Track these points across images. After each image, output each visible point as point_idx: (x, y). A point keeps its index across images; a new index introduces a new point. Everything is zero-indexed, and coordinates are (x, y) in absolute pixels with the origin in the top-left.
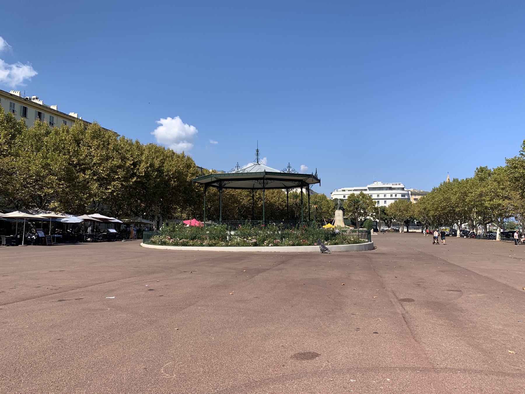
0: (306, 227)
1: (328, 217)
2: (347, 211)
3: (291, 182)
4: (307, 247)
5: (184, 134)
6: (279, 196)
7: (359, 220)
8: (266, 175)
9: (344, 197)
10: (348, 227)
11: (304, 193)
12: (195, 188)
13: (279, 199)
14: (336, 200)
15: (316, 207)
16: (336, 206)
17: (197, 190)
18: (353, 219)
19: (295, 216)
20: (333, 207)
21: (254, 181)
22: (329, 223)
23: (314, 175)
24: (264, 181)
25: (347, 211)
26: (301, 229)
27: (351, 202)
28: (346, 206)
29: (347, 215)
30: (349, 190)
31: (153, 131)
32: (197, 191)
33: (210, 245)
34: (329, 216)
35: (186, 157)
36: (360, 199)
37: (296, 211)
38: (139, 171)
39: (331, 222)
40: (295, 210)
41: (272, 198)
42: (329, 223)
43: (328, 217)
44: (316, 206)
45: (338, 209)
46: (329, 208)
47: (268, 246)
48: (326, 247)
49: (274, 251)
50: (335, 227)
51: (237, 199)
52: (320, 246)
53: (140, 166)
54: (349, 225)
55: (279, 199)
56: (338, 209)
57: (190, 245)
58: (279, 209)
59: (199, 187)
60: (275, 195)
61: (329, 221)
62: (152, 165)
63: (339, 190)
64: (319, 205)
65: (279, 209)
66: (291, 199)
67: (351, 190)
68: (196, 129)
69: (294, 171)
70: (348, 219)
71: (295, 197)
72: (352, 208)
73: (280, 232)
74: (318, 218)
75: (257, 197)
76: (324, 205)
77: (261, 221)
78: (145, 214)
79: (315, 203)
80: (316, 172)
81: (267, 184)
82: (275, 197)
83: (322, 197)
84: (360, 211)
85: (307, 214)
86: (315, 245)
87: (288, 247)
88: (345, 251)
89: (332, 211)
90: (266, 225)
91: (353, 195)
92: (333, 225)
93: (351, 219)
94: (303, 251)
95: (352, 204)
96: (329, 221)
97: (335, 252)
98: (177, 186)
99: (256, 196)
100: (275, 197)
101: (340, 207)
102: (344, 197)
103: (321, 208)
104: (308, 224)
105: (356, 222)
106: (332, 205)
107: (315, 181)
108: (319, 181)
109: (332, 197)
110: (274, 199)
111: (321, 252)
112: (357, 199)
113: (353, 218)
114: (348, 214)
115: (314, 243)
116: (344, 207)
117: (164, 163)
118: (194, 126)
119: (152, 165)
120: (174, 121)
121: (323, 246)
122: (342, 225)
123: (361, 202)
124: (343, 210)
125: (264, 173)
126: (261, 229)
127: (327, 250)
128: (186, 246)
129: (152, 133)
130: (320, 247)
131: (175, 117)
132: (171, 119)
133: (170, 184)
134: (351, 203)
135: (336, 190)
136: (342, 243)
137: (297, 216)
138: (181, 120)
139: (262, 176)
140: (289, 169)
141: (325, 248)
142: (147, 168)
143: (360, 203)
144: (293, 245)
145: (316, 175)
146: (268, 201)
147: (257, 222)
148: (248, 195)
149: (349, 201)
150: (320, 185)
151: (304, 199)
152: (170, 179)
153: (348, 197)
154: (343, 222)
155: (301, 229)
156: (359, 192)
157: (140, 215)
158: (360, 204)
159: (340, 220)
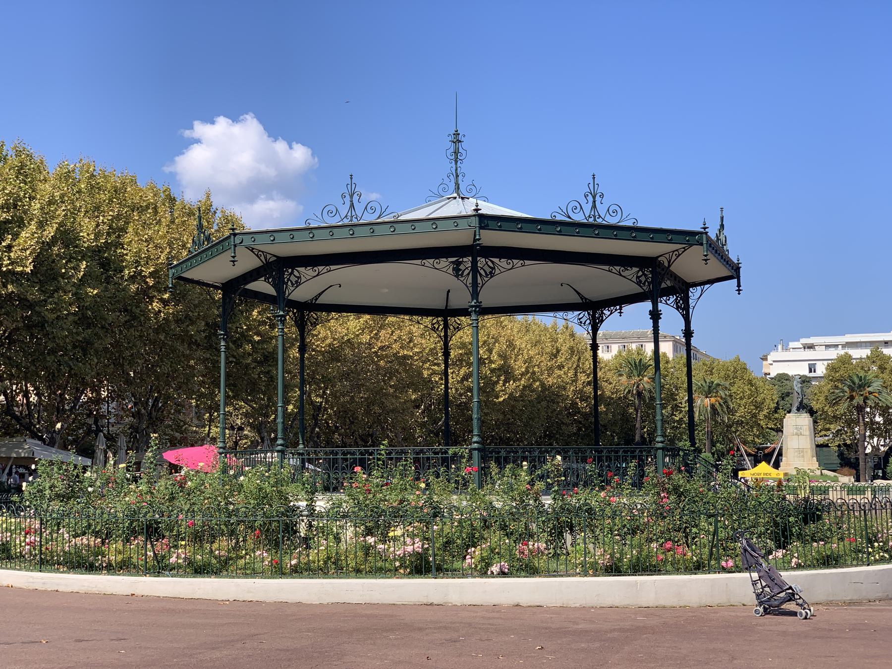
0: (679, 479)
1: (756, 440)
2: (825, 419)
3: (607, 268)
4: (690, 581)
5: (271, 173)
6: (578, 366)
7: (869, 450)
8: (481, 228)
9: (812, 369)
10: (832, 474)
11: (665, 354)
12: (249, 329)
13: (576, 375)
14: (783, 378)
15: (713, 406)
16: (783, 399)
17: (258, 336)
18: (845, 445)
19: (637, 438)
20: (773, 406)
21: (431, 261)
22: (764, 462)
23: (713, 236)
24: (474, 263)
25: (825, 419)
26: (655, 486)
27: (840, 386)
28: (822, 398)
29: (823, 433)
30: (828, 346)
31: (172, 161)
32: (257, 338)
33: (200, 570)
34: (758, 437)
35: (219, 214)
36: (870, 375)
37: (639, 419)
38: (12, 254)
39: (775, 458)
40: (637, 415)
41: (550, 370)
42: (764, 462)
43: (756, 440)
44: (713, 399)
45: (794, 409)
46: (757, 408)
47: (484, 574)
48: (784, 583)
49: (515, 602)
50: (786, 474)
51: (420, 374)
52: (755, 575)
53: (16, 236)
54: (834, 467)
55: (576, 375)
56: (794, 409)
57: (110, 568)
58: (578, 411)
59: (264, 323)
60: (560, 359)
61: (761, 454)
62: (67, 237)
63: (792, 345)
64: (721, 398)
65: (579, 413)
66: (621, 375)
67: (836, 346)
68: (313, 155)
69: (615, 211)
70: (827, 446)
71: (636, 369)
72: (842, 408)
73: (547, 501)
74: (718, 445)
75: (493, 366)
76: (741, 399)
77: (464, 450)
78: (59, 426)
79: (706, 389)
80: (722, 226)
81: (492, 274)
82: (561, 367)
83: (733, 369)
84: (871, 420)
85: (677, 427)
86: (724, 570)
87: (586, 579)
88: (880, 595)
89: (770, 419)
90: (484, 472)
91: (845, 360)
92: (777, 466)
93: (839, 446)
94: (662, 602)
95: (843, 391)
96: (761, 454)
97: (829, 603)
98: (178, 321)
99: (491, 362)
100: (561, 367)
101: (801, 402)
102: (812, 369)
103: (728, 407)
104: (687, 465)
105: (857, 459)
106: (770, 398)
107: (716, 268)
108: (734, 272)
109: (765, 370)
110: (559, 376)
111: (761, 609)
112: (862, 374)
113: (848, 442)
114: (829, 429)
115: (718, 559)
116: (815, 406)
117: (124, 230)
118: (303, 145)
119: (67, 237)
120: (237, 129)
121: (771, 578)
122: (810, 464)
123: (876, 386)
124: (812, 412)
125: (475, 222)
126: (462, 485)
127: (790, 600)
128: (91, 568)
129: (167, 169)
130: (754, 583)
131: (242, 117)
132: (230, 121)
133: (145, 313)
134: (836, 387)
135: (780, 347)
136: (858, 556)
137: (642, 437)
138: (261, 128)
139: (463, 238)
140: (594, 206)
141: (781, 586)
142: (46, 246)
143: (870, 389)
144: (614, 569)
145: (722, 237)
146: (538, 383)
147: (446, 452)
148: (459, 360)
149: (831, 380)
150: (739, 290)
151: (667, 375)
152: (145, 294)
153: (827, 369)
154: (815, 459)
155: (655, 486)
156: (865, 353)
157: (38, 430)
158: (870, 393)
159: (801, 451)
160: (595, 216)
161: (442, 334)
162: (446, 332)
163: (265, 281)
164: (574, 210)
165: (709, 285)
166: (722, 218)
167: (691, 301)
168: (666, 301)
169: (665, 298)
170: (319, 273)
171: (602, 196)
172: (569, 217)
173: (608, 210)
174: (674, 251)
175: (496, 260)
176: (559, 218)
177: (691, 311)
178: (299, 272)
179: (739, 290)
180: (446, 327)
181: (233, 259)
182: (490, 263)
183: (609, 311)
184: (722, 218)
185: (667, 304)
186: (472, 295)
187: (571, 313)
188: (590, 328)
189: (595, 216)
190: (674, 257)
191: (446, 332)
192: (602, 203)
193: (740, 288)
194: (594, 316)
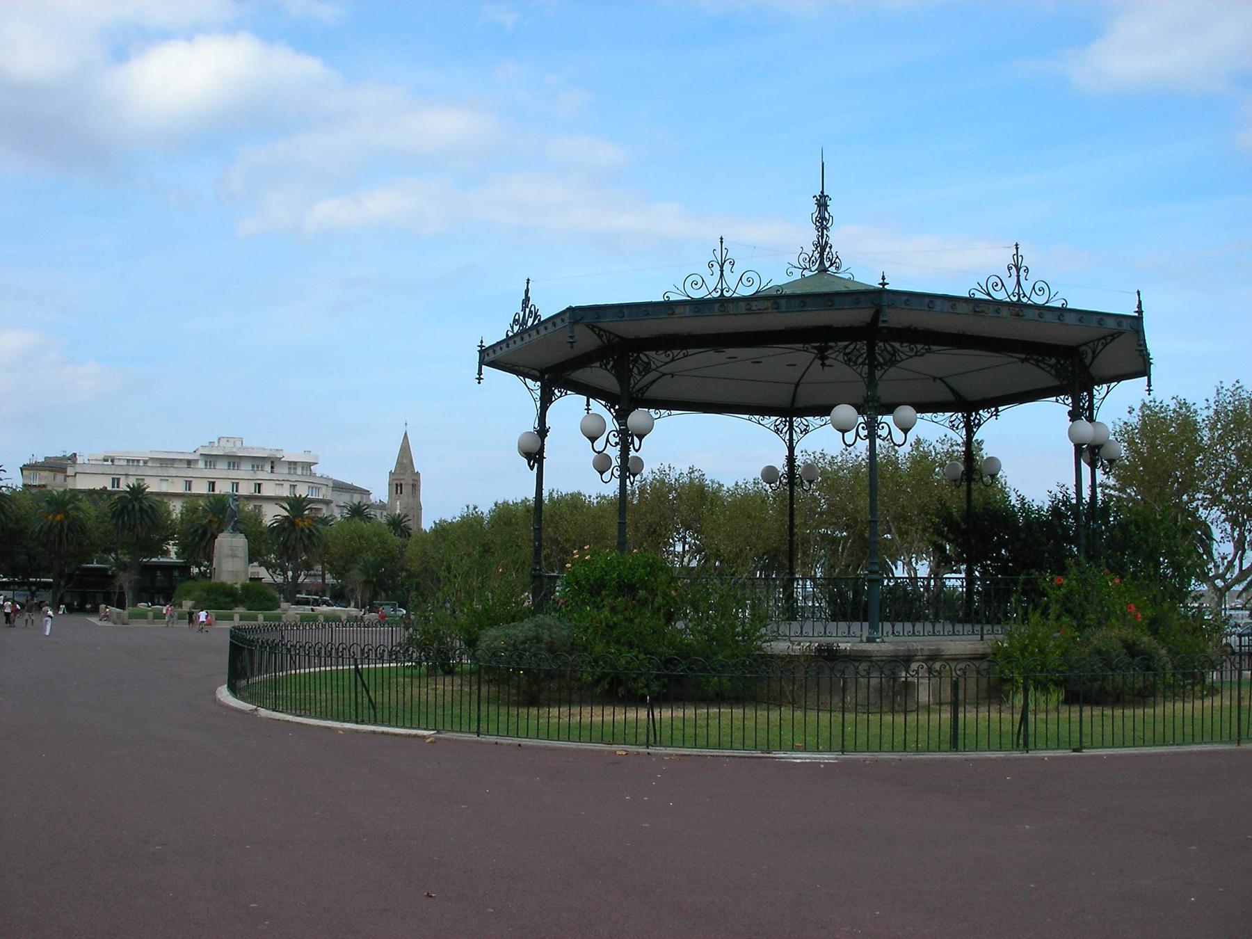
150: (480, 379)
160: (1019, 295)
161: (787, 437)
162: (791, 435)
163: (601, 367)
164: (693, 284)
165: (1116, 383)
166: (527, 291)
167: (1095, 401)
168: (1063, 401)
169: (1062, 397)
170: (673, 358)
171: (1027, 270)
172: (989, 294)
173: (1034, 288)
174: (1099, 340)
175: (897, 345)
176: (979, 295)
177: (1095, 412)
178: (648, 358)
179: (480, 379)
180: (791, 429)
181: (571, 340)
182: (889, 348)
183: (989, 413)
184: (527, 291)
185: (1065, 404)
186: (867, 387)
187: (942, 414)
188: (964, 432)
189: (1019, 295)
190: (1100, 347)
191: (791, 435)
192: (1026, 280)
193: (481, 376)
194: (968, 418)
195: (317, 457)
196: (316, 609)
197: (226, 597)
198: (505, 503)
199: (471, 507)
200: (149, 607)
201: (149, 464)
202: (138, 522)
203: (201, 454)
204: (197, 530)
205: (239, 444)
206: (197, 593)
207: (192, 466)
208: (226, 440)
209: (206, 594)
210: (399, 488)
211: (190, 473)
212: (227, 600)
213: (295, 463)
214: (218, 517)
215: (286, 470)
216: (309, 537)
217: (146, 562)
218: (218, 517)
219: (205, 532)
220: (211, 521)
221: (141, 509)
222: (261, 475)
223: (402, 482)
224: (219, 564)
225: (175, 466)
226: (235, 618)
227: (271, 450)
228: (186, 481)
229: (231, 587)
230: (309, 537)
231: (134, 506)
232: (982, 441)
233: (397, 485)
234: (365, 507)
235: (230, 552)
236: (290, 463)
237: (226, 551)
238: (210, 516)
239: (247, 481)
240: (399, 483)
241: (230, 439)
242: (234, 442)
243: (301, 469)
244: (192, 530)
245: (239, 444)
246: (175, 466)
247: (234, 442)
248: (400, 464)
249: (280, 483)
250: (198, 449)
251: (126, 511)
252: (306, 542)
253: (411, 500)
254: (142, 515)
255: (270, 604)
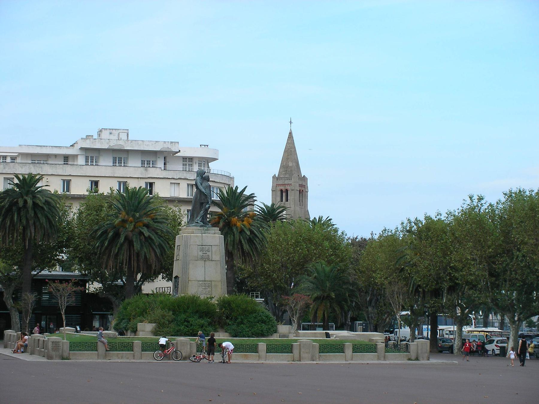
195: (216, 151)
196: (333, 335)
197: (200, 317)
198: (520, 193)
199: (476, 198)
200: (77, 331)
201: (19, 160)
202: (31, 222)
203: (82, 149)
204: (105, 232)
205: (123, 136)
206: (159, 312)
207: (70, 163)
208: (108, 131)
209: (171, 313)
210: (284, 194)
211: (68, 170)
212: (202, 322)
213: (191, 159)
214: (134, 216)
215: (180, 167)
216: (250, 241)
217: (35, 275)
218: (134, 216)
219: (117, 235)
220: (124, 221)
221: (35, 205)
222: (153, 172)
223: (288, 188)
224: (185, 269)
225: (50, 162)
226: (135, 349)
227: (165, 142)
228: (64, 181)
229: (206, 303)
230: (250, 241)
231: (25, 202)
232: (416, 219)
233: (282, 191)
234: (281, 209)
235: (201, 254)
236: (185, 159)
237: (195, 251)
238: (123, 215)
239: (137, 180)
240: (283, 188)
241: (114, 131)
242: (119, 134)
243: (197, 165)
244: (99, 233)
245: (123, 136)
246: (50, 162)
247: (119, 134)
248: (284, 167)
249: (175, 182)
250: (76, 143)
251: (14, 208)
252: (246, 247)
253: (298, 208)
254: (35, 213)
255: (264, 327)
